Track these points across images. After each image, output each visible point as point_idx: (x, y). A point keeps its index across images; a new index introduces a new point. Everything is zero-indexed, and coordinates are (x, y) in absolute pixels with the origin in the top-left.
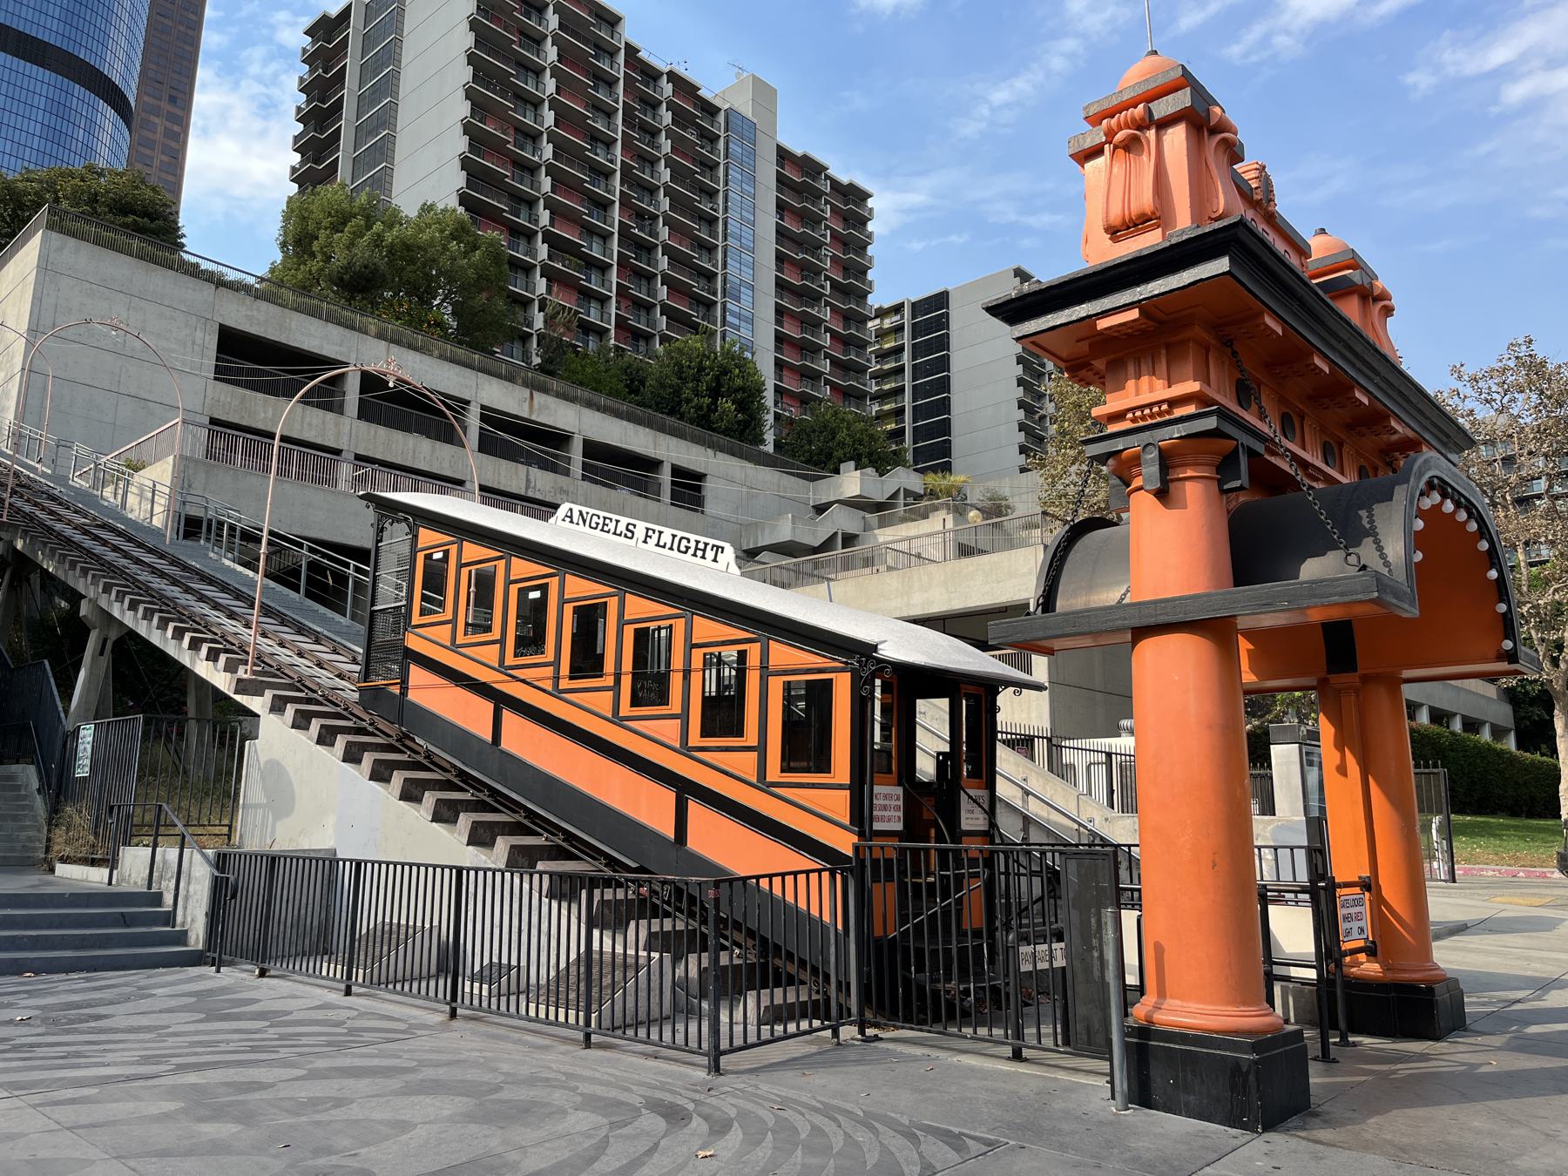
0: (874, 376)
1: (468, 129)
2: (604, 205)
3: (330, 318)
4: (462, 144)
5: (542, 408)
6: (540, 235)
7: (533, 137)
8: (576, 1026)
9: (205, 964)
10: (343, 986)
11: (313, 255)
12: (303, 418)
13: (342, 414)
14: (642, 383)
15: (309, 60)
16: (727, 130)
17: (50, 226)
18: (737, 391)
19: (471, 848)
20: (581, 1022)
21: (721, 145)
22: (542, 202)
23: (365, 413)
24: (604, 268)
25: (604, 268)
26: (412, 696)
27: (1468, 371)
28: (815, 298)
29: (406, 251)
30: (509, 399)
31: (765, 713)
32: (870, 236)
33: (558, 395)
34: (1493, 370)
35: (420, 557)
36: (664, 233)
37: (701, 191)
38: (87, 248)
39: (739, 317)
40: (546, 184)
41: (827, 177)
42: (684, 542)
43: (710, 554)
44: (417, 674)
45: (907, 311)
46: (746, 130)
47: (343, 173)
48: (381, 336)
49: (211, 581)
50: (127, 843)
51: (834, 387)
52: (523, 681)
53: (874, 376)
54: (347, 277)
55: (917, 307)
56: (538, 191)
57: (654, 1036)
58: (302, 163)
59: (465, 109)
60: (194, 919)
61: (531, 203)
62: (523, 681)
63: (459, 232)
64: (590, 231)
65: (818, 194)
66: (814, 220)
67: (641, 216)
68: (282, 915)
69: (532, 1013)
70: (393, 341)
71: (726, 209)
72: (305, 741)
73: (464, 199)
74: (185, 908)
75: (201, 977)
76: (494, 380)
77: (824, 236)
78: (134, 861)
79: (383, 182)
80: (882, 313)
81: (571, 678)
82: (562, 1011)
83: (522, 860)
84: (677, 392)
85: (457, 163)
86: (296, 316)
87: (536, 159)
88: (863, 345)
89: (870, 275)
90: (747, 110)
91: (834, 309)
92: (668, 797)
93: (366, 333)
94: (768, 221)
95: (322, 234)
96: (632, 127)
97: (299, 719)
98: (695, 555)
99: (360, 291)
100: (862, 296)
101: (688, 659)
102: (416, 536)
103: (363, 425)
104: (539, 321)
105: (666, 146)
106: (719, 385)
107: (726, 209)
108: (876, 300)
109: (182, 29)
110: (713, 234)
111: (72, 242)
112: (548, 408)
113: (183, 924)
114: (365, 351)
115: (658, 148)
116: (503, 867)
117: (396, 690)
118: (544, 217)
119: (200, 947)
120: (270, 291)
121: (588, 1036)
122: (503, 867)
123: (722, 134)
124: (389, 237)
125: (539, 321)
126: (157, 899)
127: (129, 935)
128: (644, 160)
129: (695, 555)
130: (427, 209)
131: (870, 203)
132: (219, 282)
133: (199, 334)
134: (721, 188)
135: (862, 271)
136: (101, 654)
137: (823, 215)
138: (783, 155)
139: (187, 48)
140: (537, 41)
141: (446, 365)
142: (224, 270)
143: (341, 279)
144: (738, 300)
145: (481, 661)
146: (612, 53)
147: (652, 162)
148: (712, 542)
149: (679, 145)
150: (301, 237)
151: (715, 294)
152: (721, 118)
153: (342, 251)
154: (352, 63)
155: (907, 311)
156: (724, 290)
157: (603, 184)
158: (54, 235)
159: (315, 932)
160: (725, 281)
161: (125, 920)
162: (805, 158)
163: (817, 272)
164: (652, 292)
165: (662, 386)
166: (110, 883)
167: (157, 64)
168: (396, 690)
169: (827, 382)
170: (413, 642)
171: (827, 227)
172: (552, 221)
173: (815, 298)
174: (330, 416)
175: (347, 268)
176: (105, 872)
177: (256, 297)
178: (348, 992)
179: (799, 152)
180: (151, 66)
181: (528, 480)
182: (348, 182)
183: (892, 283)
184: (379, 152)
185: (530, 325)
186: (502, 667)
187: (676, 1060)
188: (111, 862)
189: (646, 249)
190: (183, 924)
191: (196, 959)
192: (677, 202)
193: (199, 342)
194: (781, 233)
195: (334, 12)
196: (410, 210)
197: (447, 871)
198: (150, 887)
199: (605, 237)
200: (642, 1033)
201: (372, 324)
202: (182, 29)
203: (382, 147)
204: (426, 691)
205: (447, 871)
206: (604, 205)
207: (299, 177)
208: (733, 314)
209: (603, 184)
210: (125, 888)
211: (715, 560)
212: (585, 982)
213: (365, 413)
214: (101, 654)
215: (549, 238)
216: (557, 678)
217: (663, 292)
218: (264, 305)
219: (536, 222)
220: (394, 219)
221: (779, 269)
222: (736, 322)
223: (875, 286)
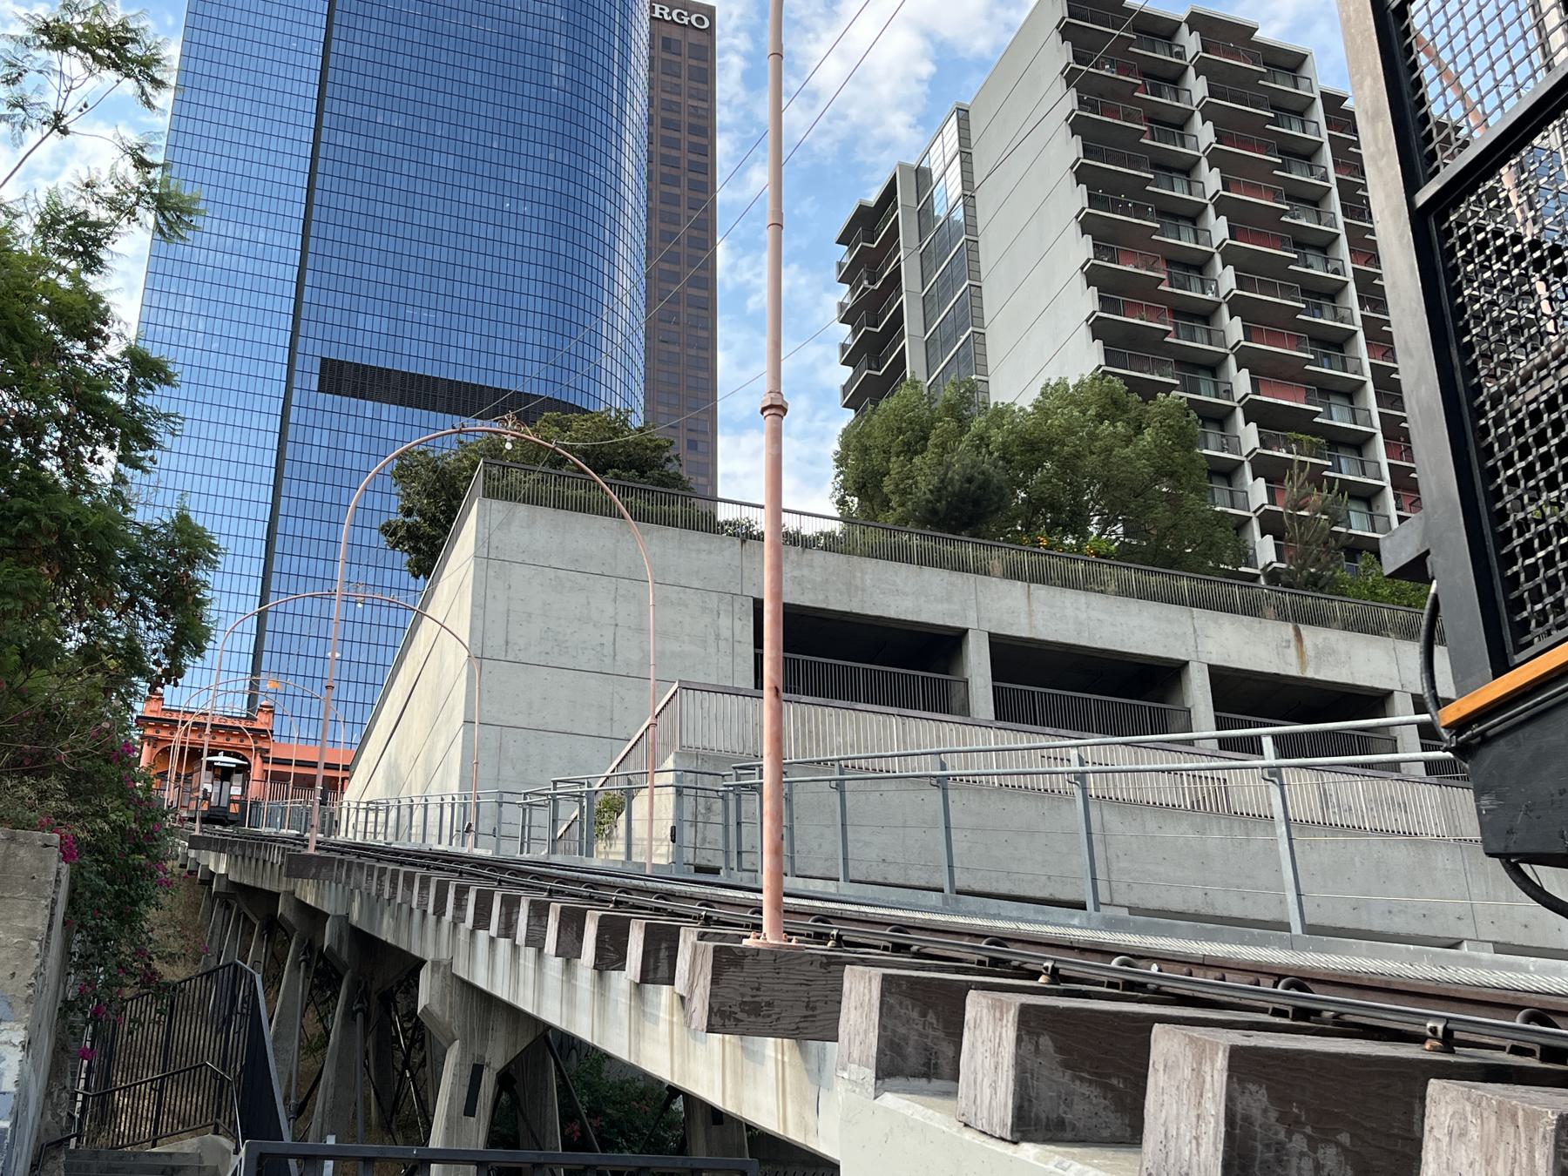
1: (1093, 276)
3: (925, 560)
4: (1087, 301)
5: (1323, 654)
7: (1198, 266)
11: (886, 504)
15: (849, 276)
17: (490, 493)
23: (1007, 710)
29: (1031, 444)
33: (1347, 626)
38: (545, 516)
40: (1234, 329)
47: (914, 365)
48: (1013, 574)
56: (1223, 343)
59: (1083, 249)
63: (1112, 407)
64: (1328, 390)
70: (1033, 579)
76: (1225, 618)
79: (974, 355)
86: (870, 564)
87: (1210, 296)
95: (895, 465)
97: (1055, 1079)
109: (692, 352)
111: (522, 510)
112: (1333, 652)
114: (990, 603)
118: (1241, 382)
124: (997, 437)
133: (724, 622)
136: (470, 1110)
139: (702, 374)
140: (1178, 124)
141: (1134, 605)
143: (934, 512)
146: (1300, 109)
150: (864, 479)
153: (924, 473)
154: (907, 259)
157: (1327, 311)
158: (497, 505)
167: (668, 404)
175: (938, 491)
180: (660, 409)
182: (921, 376)
184: (962, 325)
193: (726, 633)
195: (872, 198)
202: (692, 352)
203: (967, 355)
213: (1007, 710)
214: (470, 1110)
215: (1254, 412)
219: (1229, 393)
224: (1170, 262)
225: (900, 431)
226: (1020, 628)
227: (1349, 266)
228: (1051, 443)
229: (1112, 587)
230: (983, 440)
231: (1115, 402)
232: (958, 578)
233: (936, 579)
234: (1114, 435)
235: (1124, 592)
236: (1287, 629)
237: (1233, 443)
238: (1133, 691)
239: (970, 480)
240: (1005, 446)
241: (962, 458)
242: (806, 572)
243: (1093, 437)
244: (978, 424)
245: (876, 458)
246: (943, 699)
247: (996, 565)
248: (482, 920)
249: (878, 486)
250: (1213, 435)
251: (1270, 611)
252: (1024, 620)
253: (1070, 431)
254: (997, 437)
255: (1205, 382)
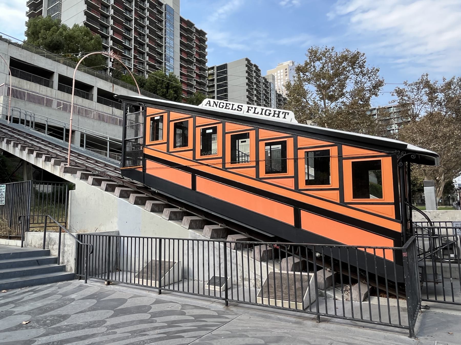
0: (208, 86)
2: (129, 30)
3: (48, 57)
6: (110, 38)
8: (156, 288)
9: (76, 279)
10: (158, 290)
12: (40, 88)
13: (52, 88)
14: (144, 84)
16: (165, 11)
18: (174, 87)
19: (190, 230)
20: (158, 286)
21: (164, 15)
22: (110, 27)
24: (130, 50)
25: (130, 50)
26: (148, 172)
27: (409, 83)
28: (191, 63)
30: (107, 86)
31: (342, 172)
32: (206, 46)
33: (121, 86)
34: (417, 83)
35: (148, 119)
36: (147, 40)
37: (158, 28)
39: (169, 67)
40: (111, 22)
41: (194, 28)
42: (268, 112)
43: (282, 116)
44: (149, 163)
45: (215, 69)
46: (171, 11)
49: (31, 136)
50: (28, 230)
51: (197, 89)
52: (207, 165)
53: (208, 86)
54: (51, 45)
55: (219, 68)
57: (176, 289)
58: (30, 11)
60: (69, 261)
61: (107, 27)
62: (207, 165)
63: (87, 34)
64: (126, 38)
65: (192, 32)
66: (191, 40)
67: (140, 34)
68: (101, 258)
69: (137, 282)
70: (68, 66)
71: (165, 35)
72: (100, 191)
73: (85, 24)
74: (63, 257)
75: (80, 288)
77: (194, 45)
78: (34, 239)
80: (209, 69)
81: (231, 163)
82: (149, 281)
83: (216, 235)
84: (156, 87)
85: (83, 13)
87: (108, 14)
88: (204, 77)
89: (207, 57)
90: (171, 5)
91: (197, 67)
92: (290, 210)
93: (59, 62)
94: (178, 39)
95: (42, 31)
96: (137, 7)
97: (95, 182)
98: (274, 116)
99: (55, 50)
100: (204, 63)
101: (296, 154)
102: (146, 111)
103: (60, 92)
104: (110, 65)
105: (148, 14)
106: (169, 86)
107: (165, 35)
108: (208, 65)
110: (162, 42)
113: (63, 263)
115: (145, 14)
116: (208, 238)
117: (141, 170)
118: (111, 32)
119: (73, 272)
120: (25, 47)
121: (160, 291)
122: (208, 238)
123: (164, 12)
124: (65, 33)
125: (110, 65)
126: (48, 253)
127: (39, 269)
128: (141, 17)
129: (274, 116)
130: (76, 26)
131: (206, 36)
132: (10, 43)
134: (164, 28)
135: (204, 56)
137: (193, 39)
138: (182, 20)
142: (11, 39)
143: (49, 46)
144: (169, 62)
145: (184, 157)
147: (143, 18)
148: (282, 111)
149: (151, 13)
150: (33, 32)
151: (162, 60)
152: (164, 7)
153: (50, 36)
155: (215, 69)
156: (165, 59)
157: (128, 24)
159: (114, 263)
160: (165, 56)
161: (38, 263)
162: (188, 21)
163: (192, 55)
164: (144, 58)
165: (151, 85)
166: (22, 246)
168: (141, 170)
169: (195, 88)
170: (147, 151)
171: (194, 42)
172: (113, 33)
173: (191, 63)
174: (49, 89)
175: (51, 42)
176: (19, 243)
177: (22, 48)
178: (160, 293)
179: (186, 19)
181: (113, 112)
183: (212, 61)
185: (107, 66)
186: (194, 159)
187: (189, 297)
188: (21, 238)
189: (142, 45)
190: (63, 263)
191: (71, 277)
192: (151, 31)
194: (181, 43)
196: (70, 26)
197: (154, 240)
198: (44, 248)
199: (130, 40)
200: (171, 288)
201: (62, 60)
204: (153, 169)
205: (154, 240)
206: (129, 30)
207: (30, 16)
208: (168, 66)
209: (128, 24)
210: (29, 249)
211: (284, 118)
212: (271, 287)
216: (224, 163)
217: (147, 58)
218: (25, 51)
219: (109, 34)
220: (65, 28)
221: (181, 54)
222: (169, 68)
223: (208, 60)
224: (102, 4)
225: (44, 25)
226: (65, 74)
227: (134, 25)
228: (75, 38)
229: (83, 70)
230: (61, 34)
231: (88, 33)
232: (54, 62)
233: (49, 61)
234: (87, 39)
235: (85, 72)
236: (112, 84)
237: (107, 43)
238: (84, 90)
239: (58, 42)
240: (65, 37)
241: (56, 37)
242: (22, 54)
243: (83, 38)
244: (61, 30)
245: (38, 28)
246: (48, 84)
247: (62, 61)
248: (57, 202)
249: (38, 34)
250: (104, 40)
251: (109, 81)
252: (66, 73)
253: (78, 36)
254: (65, 33)
255: (105, 30)
